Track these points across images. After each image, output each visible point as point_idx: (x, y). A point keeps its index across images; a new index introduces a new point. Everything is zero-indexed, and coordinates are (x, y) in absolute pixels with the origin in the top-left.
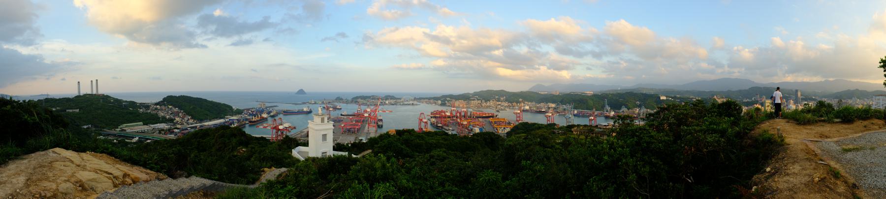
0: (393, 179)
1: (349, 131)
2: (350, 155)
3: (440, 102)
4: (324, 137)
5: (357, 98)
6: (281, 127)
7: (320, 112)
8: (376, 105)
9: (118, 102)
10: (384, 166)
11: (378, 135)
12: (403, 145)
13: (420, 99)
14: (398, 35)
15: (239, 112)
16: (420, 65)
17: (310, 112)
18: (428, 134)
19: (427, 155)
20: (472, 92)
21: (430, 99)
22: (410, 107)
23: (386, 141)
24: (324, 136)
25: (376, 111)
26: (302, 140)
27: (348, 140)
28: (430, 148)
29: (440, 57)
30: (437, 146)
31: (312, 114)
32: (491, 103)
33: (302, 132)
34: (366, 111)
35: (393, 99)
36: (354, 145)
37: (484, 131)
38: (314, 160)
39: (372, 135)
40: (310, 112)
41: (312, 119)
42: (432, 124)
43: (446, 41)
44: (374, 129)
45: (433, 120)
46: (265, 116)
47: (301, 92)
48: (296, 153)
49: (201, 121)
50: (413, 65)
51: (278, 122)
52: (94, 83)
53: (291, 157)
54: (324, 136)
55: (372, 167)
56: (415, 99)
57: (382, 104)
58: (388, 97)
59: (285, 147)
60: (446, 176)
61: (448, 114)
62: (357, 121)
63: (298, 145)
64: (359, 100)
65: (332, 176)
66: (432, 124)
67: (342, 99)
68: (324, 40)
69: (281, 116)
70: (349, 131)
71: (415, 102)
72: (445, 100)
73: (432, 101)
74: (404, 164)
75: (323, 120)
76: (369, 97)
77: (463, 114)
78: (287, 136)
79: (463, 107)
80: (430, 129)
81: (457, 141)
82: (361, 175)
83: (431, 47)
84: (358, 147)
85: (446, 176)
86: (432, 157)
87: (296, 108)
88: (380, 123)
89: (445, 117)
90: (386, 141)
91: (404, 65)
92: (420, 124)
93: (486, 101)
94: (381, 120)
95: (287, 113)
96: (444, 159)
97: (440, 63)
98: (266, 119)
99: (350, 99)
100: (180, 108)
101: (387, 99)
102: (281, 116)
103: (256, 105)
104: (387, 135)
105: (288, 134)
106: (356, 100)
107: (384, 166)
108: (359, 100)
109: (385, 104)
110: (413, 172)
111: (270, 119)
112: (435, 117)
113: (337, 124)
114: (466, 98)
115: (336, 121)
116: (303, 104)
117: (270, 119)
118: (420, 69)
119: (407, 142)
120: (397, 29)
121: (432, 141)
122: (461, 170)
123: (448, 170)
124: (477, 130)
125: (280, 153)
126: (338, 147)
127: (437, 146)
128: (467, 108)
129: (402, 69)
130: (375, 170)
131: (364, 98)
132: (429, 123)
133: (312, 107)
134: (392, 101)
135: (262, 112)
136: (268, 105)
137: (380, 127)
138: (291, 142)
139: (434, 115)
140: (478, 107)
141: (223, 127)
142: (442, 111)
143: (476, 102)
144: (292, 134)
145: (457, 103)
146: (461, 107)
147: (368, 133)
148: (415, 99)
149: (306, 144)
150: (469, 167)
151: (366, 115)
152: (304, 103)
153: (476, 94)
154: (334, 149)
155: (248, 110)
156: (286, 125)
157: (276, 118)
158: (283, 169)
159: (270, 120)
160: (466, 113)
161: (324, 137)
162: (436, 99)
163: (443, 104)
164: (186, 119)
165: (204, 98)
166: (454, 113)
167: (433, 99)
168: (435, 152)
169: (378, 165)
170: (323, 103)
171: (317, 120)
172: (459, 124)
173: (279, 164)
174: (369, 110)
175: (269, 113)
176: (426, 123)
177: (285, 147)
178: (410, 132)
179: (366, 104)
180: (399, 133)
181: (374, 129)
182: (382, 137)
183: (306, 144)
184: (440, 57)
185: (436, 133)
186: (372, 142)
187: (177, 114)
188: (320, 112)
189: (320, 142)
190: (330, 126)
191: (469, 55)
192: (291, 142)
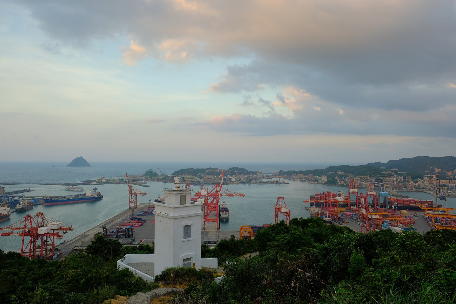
3: (324, 178)
6: (42, 231)
8: (218, 185)
13: (290, 174)
20: (384, 160)
21: (306, 173)
24: (187, 228)
32: (426, 181)
35: (244, 175)
47: (79, 162)
51: (37, 220)
54: (187, 228)
56: (281, 173)
61: (340, 199)
67: (155, 174)
71: (282, 179)
73: (310, 176)
77: (370, 201)
88: (224, 215)
89: (335, 204)
92: (277, 216)
93: (415, 178)
95: (50, 202)
112: (319, 205)
133: (101, 189)
134: (243, 178)
137: (225, 221)
139: (316, 201)
140: (400, 189)
142: (329, 195)
153: (392, 164)
157: (33, 213)
160: (376, 198)
166: (353, 199)
174: (204, 193)
179: (197, 183)
189: (173, 247)
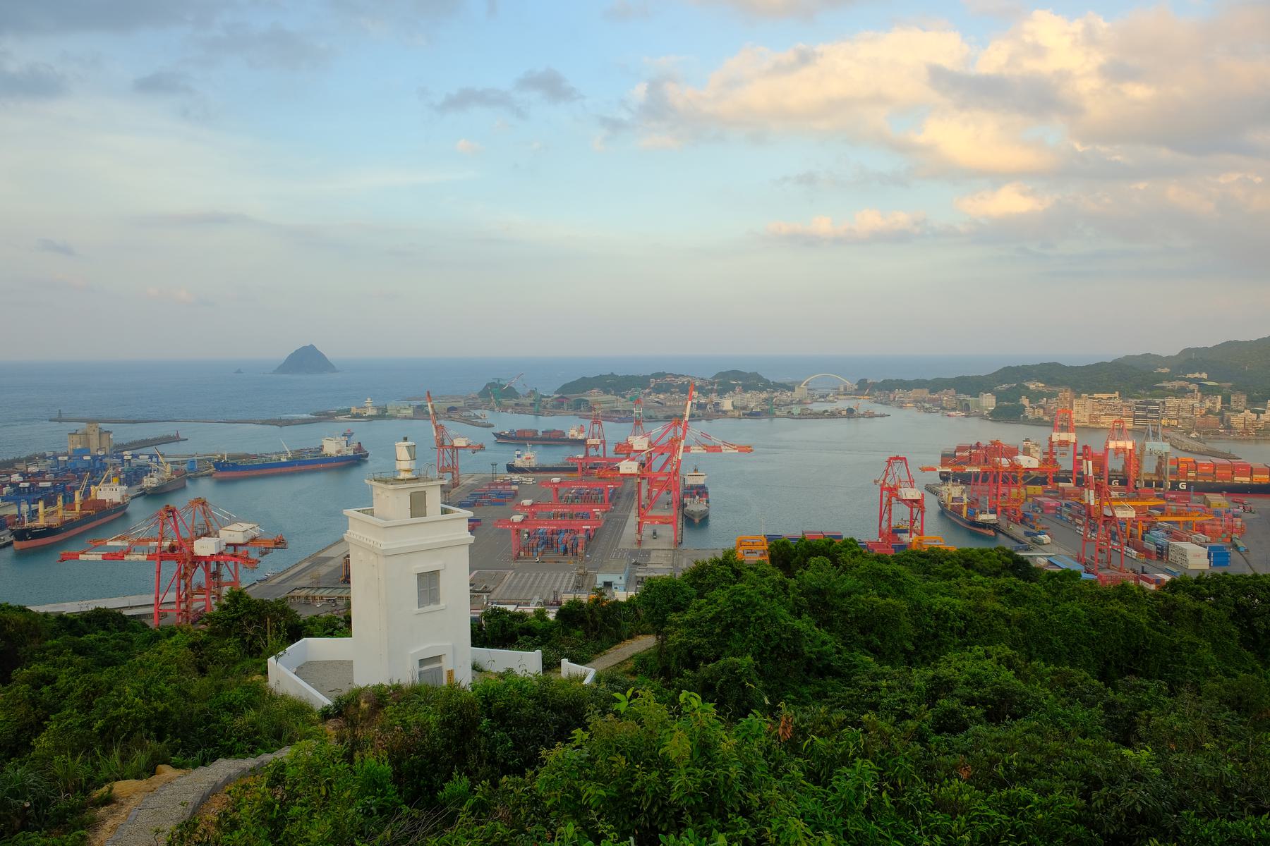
0: (746, 812)
1: (549, 546)
2: (550, 665)
3: (988, 401)
4: (429, 584)
5: (585, 384)
6: (204, 547)
7: (404, 463)
8: (675, 419)
10: (704, 749)
11: (686, 564)
12: (793, 629)
13: (886, 388)
14: (801, 90)
16: (901, 218)
17: (357, 460)
18: (929, 562)
19: (920, 677)
20: (1169, 347)
21: (936, 386)
22: (840, 427)
23: (721, 596)
25: (673, 446)
27: (539, 591)
28: (932, 637)
29: (996, 178)
30: (971, 630)
31: (362, 477)
33: (318, 561)
34: (625, 450)
35: (755, 389)
36: (571, 616)
37: (1238, 567)
38: (380, 698)
39: (662, 566)
40: (357, 460)
41: (364, 502)
42: (948, 513)
43: (1036, 98)
44: (667, 532)
45: (954, 491)
46: (110, 493)
47: (307, 360)
48: (289, 673)
50: (869, 218)
51: (189, 519)
53: (259, 696)
55: (646, 754)
56: (864, 387)
57: (705, 413)
58: (730, 380)
59: (230, 647)
60: (1011, 807)
61: (1029, 462)
62: (585, 498)
63: (296, 632)
64: (595, 396)
65: (459, 784)
66: (948, 513)
67: (511, 393)
68: (464, 99)
69: (204, 488)
70: (549, 543)
71: (863, 404)
72: (1015, 389)
73: (947, 397)
74: (801, 732)
75: (418, 506)
76: (642, 382)
78: (237, 597)
79: (1119, 432)
80: (934, 535)
81: (1073, 607)
82: (593, 792)
83: (961, 136)
84: (586, 626)
85: (1011, 807)
86: (941, 687)
87: (282, 443)
88: (695, 506)
89: (1015, 476)
90: (721, 596)
91: (823, 224)
94: (701, 491)
95: (232, 470)
96: (1001, 708)
97: (1011, 202)
98: (118, 512)
99: (549, 390)
101: (724, 389)
102: (204, 488)
103: (54, 440)
104: (729, 569)
105: (246, 580)
106: (576, 393)
107: (704, 749)
108: (595, 396)
109: (719, 413)
110: (845, 780)
111: (139, 509)
112: (965, 479)
113: (490, 513)
114: (1133, 379)
115: (481, 501)
116: (316, 419)
117: (139, 509)
118: (899, 237)
119: (820, 604)
120: (805, 59)
121: (948, 599)
122: (1091, 783)
123: (1024, 776)
124: (1196, 558)
125: (199, 684)
126: (494, 631)
127: (971, 630)
128: (1138, 433)
129: (809, 241)
130: (666, 765)
131: (617, 384)
132: (931, 504)
133: (365, 434)
134: (753, 400)
135: (96, 471)
136: (123, 433)
137: (696, 522)
138: (261, 624)
139: (956, 467)
140: (1207, 433)
142: (996, 449)
143: (1195, 404)
144: (262, 580)
145: (1082, 410)
146: (1104, 431)
147: (639, 557)
148: (864, 387)
149: (338, 625)
150: (1138, 777)
151: (628, 467)
152: (325, 417)
153: (1192, 360)
154: (481, 637)
156: (235, 533)
158: (224, 768)
159: (142, 518)
160: (1132, 459)
161: (429, 584)
162: (969, 386)
163: (1008, 413)
166: (1066, 464)
167: (954, 389)
168: (958, 665)
169: (677, 745)
170: (420, 412)
171: (392, 502)
172: (1091, 517)
173: (193, 738)
174: (639, 443)
175: (133, 477)
176: (916, 504)
177: (230, 647)
178: (832, 550)
180: (787, 555)
181: (667, 532)
182: (701, 577)
184: (996, 178)
185: (968, 562)
186: (659, 603)
188: (404, 463)
189: (406, 611)
190: (451, 533)
191: (1164, 154)
192: (261, 624)
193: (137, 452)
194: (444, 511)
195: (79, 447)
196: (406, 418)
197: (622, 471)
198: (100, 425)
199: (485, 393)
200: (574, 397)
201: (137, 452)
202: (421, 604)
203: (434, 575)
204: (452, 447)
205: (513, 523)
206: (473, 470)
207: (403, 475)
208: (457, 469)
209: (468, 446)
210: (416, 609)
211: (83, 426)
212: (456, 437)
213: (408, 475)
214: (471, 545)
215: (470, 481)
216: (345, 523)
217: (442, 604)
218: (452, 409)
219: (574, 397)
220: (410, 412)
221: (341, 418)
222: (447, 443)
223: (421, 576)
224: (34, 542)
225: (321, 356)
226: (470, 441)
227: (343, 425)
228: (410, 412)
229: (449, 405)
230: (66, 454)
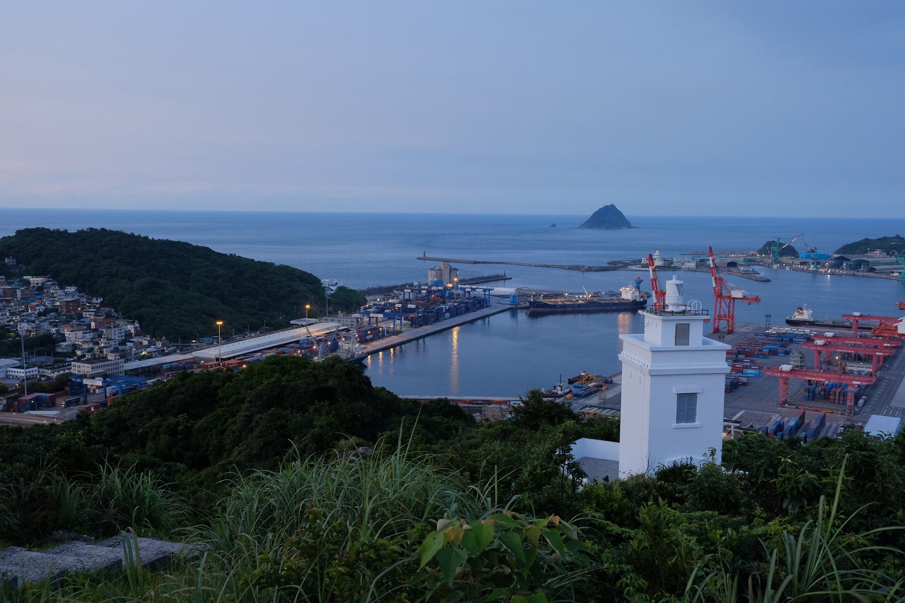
5: (865, 245)
9: (62, 235)
15: (347, 301)
26: (589, 407)
41: (638, 328)
49: (182, 339)
52: (421, 349)
64: (877, 256)
67: (790, 251)
75: (682, 334)
99: (830, 246)
100: (87, 286)
116: (606, 271)
141: (281, 363)
149: (611, 433)
155: (387, 291)
164: (116, 335)
165: (195, 239)
183: (611, 433)
187: (71, 315)
189: (661, 410)
190: (711, 361)
193: (474, 287)
194: (704, 343)
195: (435, 279)
196: (689, 269)
197: (900, 331)
198: (451, 264)
199: (766, 249)
200: (854, 258)
201: (474, 287)
202: (679, 420)
203: (693, 396)
204: (729, 297)
205: (782, 372)
206: (747, 320)
207: (670, 309)
208: (733, 318)
209: (744, 298)
210: (674, 424)
211: (441, 265)
212: (733, 289)
213: (675, 309)
214: (727, 375)
215: (744, 330)
216: (617, 347)
217: (697, 423)
218: (733, 264)
219: (854, 258)
220: (692, 265)
221: (633, 268)
222: (725, 293)
223: (680, 396)
224: (839, 601)
225: (620, 214)
226: (747, 293)
227: (634, 273)
228: (692, 265)
229: (729, 260)
230: (426, 285)
